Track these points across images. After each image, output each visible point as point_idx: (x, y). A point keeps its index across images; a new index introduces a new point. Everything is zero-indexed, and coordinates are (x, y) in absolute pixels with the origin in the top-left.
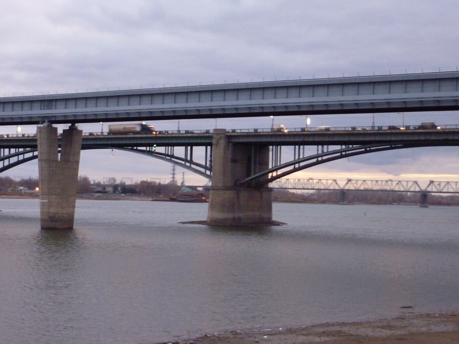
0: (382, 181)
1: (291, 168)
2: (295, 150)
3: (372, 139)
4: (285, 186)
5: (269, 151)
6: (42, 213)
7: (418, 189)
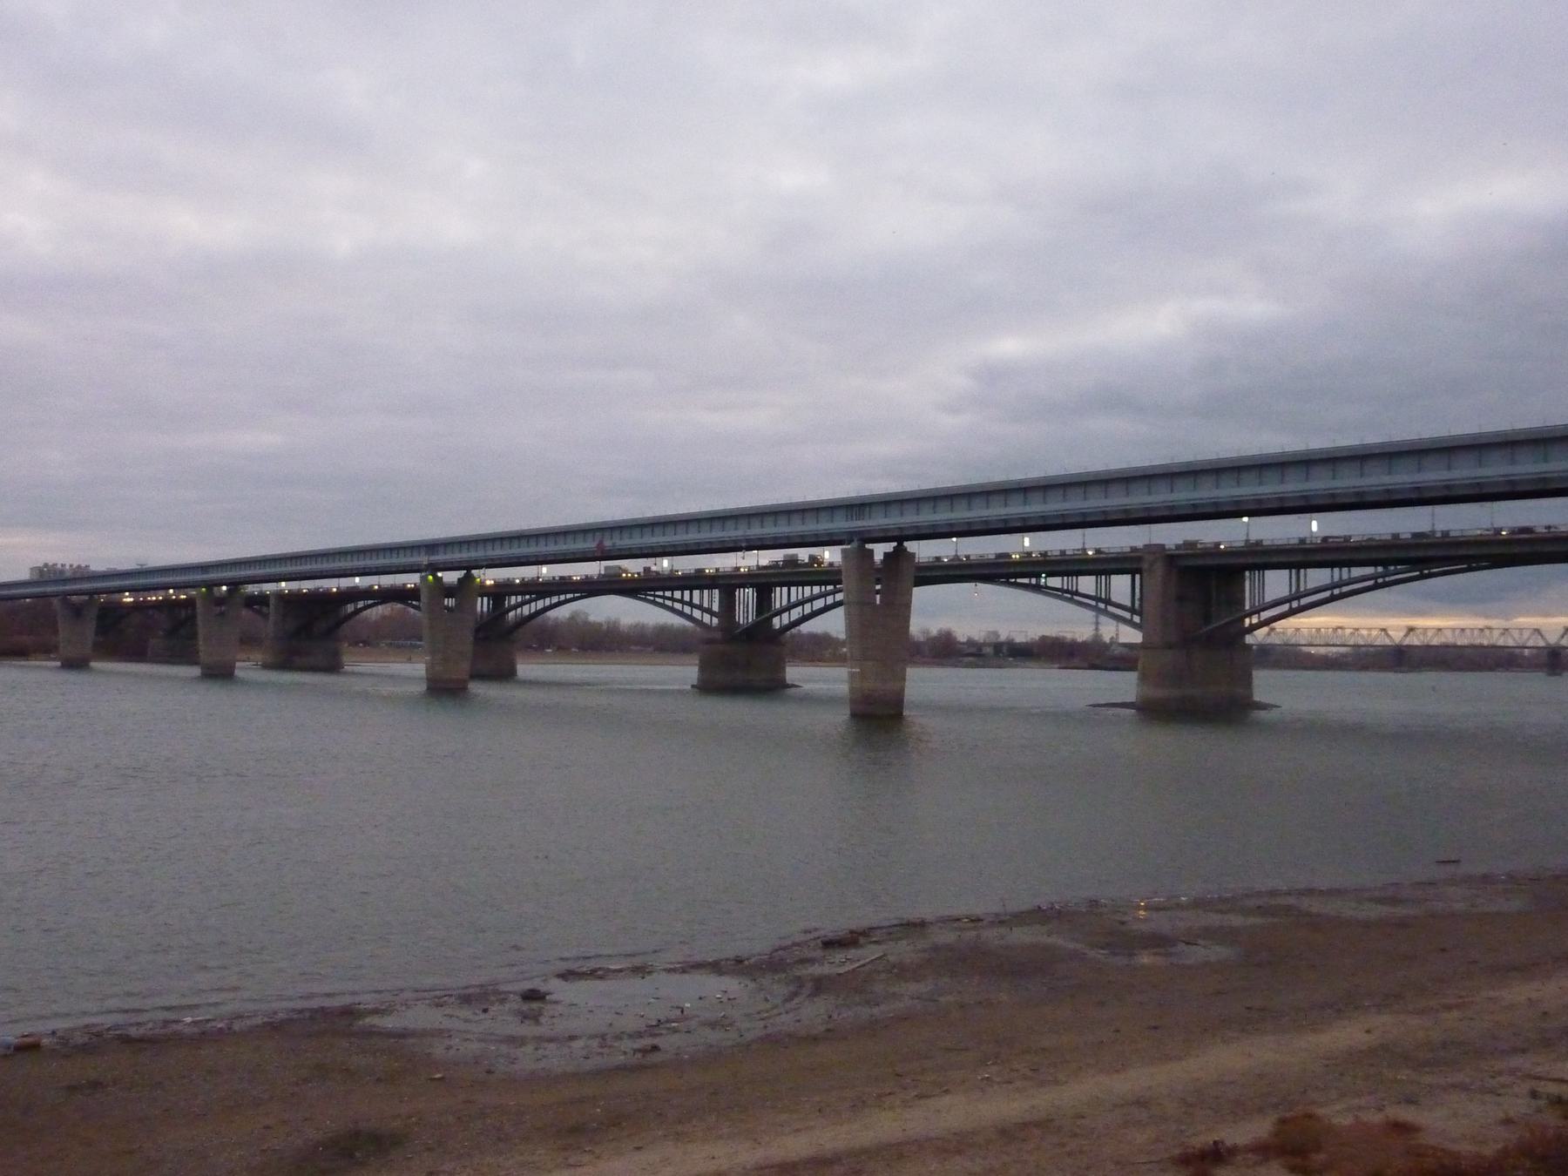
0: (1472, 629)
1: (1285, 607)
2: (1291, 578)
3: (1431, 553)
4: (1293, 641)
5: (1245, 580)
6: (852, 690)
7: (1542, 644)
